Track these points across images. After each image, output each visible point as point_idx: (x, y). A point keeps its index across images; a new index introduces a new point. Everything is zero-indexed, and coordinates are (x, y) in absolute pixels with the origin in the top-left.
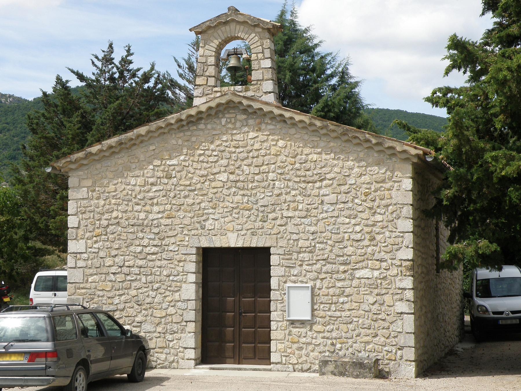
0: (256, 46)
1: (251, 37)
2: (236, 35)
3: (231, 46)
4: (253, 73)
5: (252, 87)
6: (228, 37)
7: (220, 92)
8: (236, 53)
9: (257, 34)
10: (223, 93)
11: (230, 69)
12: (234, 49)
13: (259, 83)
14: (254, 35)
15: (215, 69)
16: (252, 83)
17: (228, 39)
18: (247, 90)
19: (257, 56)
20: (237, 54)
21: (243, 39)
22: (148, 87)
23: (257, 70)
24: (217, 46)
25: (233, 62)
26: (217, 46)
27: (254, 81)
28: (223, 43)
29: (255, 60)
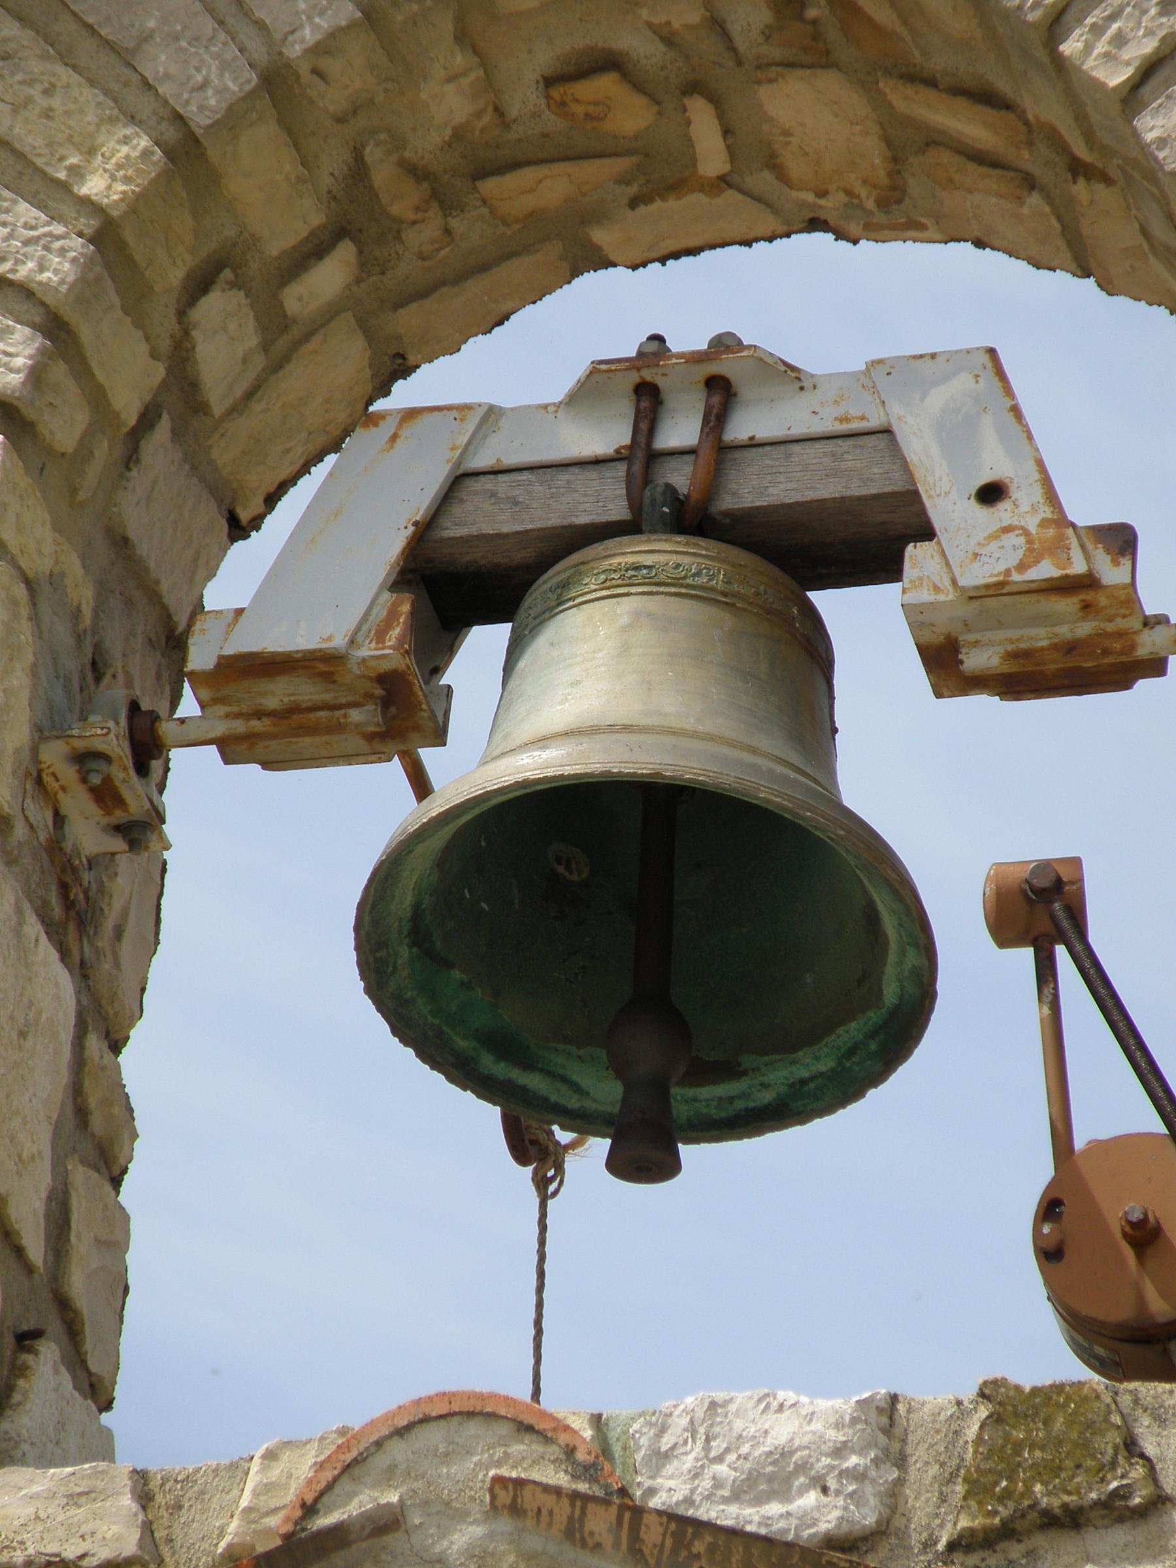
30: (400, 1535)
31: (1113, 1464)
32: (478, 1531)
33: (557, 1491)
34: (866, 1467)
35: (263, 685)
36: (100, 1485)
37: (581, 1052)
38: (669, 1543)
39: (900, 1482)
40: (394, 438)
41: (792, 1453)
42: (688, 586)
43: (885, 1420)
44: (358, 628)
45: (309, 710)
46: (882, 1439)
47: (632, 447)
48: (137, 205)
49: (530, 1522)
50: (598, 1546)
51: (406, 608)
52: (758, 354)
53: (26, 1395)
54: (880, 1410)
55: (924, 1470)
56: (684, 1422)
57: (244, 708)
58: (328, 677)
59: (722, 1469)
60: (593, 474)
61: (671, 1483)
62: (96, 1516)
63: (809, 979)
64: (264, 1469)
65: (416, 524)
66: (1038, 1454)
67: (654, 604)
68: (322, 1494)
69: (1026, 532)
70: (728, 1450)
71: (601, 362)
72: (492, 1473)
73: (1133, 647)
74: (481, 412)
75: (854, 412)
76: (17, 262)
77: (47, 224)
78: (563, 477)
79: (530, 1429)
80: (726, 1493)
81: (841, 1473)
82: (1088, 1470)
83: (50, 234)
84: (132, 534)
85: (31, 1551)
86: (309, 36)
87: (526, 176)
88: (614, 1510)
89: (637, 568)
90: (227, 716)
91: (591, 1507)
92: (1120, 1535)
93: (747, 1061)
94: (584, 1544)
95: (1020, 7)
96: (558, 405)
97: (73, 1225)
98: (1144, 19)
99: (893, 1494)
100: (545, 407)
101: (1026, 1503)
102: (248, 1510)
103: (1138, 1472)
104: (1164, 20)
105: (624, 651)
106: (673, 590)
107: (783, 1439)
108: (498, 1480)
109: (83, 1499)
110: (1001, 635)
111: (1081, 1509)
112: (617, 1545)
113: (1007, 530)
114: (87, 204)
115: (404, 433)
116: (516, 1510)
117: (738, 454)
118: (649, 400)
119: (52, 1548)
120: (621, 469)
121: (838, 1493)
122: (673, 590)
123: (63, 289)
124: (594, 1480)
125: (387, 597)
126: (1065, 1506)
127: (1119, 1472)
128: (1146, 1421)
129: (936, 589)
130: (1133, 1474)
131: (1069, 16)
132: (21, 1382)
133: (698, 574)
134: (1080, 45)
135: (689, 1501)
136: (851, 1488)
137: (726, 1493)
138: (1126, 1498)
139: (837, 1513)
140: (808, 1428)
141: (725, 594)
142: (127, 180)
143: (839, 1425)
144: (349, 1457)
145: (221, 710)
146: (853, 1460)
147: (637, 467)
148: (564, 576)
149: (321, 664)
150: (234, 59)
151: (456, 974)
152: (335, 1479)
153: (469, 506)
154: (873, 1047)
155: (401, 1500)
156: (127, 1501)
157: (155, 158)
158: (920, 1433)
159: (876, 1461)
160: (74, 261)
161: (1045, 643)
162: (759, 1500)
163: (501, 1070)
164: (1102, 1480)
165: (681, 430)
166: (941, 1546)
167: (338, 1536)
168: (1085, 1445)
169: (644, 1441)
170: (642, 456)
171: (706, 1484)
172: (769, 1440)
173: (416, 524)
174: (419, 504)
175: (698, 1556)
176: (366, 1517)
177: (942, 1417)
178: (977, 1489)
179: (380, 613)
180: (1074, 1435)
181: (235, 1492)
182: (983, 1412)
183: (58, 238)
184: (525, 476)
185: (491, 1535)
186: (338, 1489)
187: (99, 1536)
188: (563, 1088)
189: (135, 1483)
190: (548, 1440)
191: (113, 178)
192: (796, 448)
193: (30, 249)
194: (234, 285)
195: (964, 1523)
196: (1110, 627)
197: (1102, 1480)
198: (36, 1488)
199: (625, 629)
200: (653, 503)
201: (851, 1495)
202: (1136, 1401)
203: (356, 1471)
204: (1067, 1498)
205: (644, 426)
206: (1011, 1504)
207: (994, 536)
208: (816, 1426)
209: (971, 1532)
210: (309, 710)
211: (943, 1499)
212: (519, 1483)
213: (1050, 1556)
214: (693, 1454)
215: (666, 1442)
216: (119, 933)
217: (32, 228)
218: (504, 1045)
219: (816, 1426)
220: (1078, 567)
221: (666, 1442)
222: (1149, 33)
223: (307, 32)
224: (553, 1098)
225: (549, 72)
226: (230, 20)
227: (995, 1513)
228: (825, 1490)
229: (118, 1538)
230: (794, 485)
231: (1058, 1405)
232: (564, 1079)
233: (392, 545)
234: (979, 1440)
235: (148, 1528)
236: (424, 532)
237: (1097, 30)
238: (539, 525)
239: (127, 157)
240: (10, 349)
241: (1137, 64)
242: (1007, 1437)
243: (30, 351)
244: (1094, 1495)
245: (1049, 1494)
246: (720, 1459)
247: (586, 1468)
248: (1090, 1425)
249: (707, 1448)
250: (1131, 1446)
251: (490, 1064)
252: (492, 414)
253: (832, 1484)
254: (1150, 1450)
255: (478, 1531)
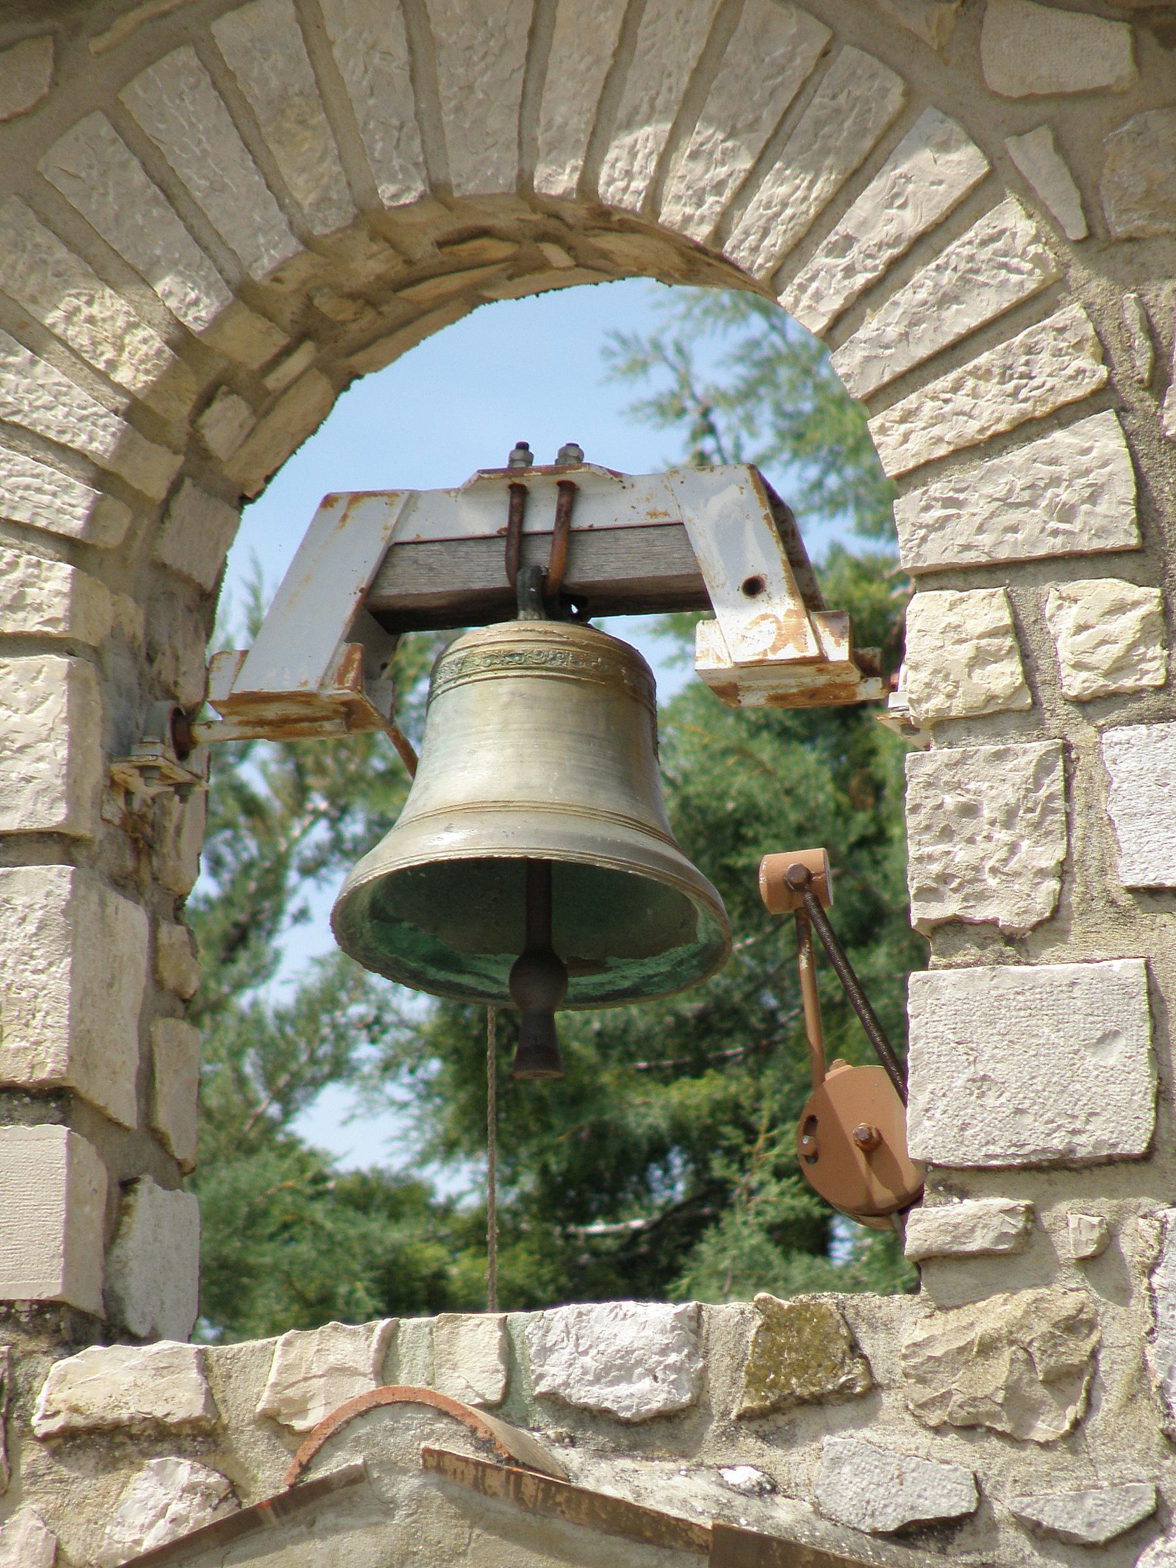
0: (992, 408)
1: (882, 217)
2: (558, 180)
3: (434, 423)
4: (940, 1001)
5: (904, 1329)
6: (372, 221)
7: (202, 1437)
8: (553, 572)
9: (1034, 154)
10: (270, 1477)
11: (422, 920)
12: (515, 483)
13: (1074, 1224)
14: (961, 165)
15: (79, 930)
16: (925, 1227)
17: (369, 264)
18: (802, 1396)
19: (1023, 638)
20: (566, 601)
21: (697, 263)
22: (255, 1004)
23: (1017, 943)
24: (137, 414)
25: (486, 769)
26: (137, 414)
27: (958, 1180)
28: (250, 343)
29: (988, 718)
30: (365, 1484)
31: (843, 1363)
32: (416, 1482)
33: (466, 1460)
34: (682, 1362)
35: (263, 706)
36: (176, 1361)
37: (498, 958)
38: (540, 1495)
39: (705, 1369)
40: (344, 518)
41: (633, 1352)
42: (547, 669)
43: (694, 1324)
44: (326, 674)
45: (296, 721)
46: (693, 1337)
47: (508, 530)
48: (153, 389)
49: (449, 1478)
50: (494, 1494)
51: (357, 656)
52: (593, 469)
53: (130, 1228)
54: (690, 1318)
55: (720, 1362)
56: (562, 1326)
57: (251, 718)
58: (308, 703)
59: (587, 1360)
60: (483, 547)
61: (553, 1370)
62: (175, 1385)
63: (649, 912)
64: (284, 1353)
65: (362, 590)
66: (794, 1355)
67: (522, 685)
68: (312, 1456)
69: (777, 621)
70: (591, 1347)
71: (485, 471)
72: (423, 1445)
73: (854, 695)
74: (404, 497)
75: (660, 509)
76: (74, 434)
77: (94, 405)
78: (463, 549)
79: (446, 1414)
80: (590, 1377)
81: (666, 1367)
82: (826, 1368)
83: (95, 414)
84: (167, 562)
85: (132, 1410)
86: (267, 263)
87: (432, 282)
88: (503, 1474)
89: (512, 656)
90: (240, 723)
91: (488, 1471)
92: (849, 1410)
93: (612, 961)
94: (485, 1493)
95: (750, 269)
96: (457, 490)
97: (157, 1075)
98: (834, 281)
99: (702, 1377)
100: (448, 492)
101: (787, 1392)
102: (275, 1385)
103: (859, 1369)
104: (846, 282)
105: (505, 726)
106: (537, 673)
107: (626, 1342)
108: (427, 1451)
109: (165, 1372)
110: (764, 683)
111: (823, 1395)
112: (507, 1494)
113: (764, 617)
114: (118, 388)
115: (351, 513)
116: (440, 1469)
117: (582, 537)
118: (520, 496)
119: (146, 1409)
120: (502, 545)
121: (664, 1381)
122: (537, 673)
123: (107, 456)
124: (489, 1451)
125: (345, 647)
126: (812, 1394)
127: (846, 1369)
128: (864, 1327)
129: (719, 658)
130: (856, 1371)
131: (784, 274)
132: (126, 1219)
133: (554, 659)
134: (791, 299)
135: (566, 1384)
136: (673, 1377)
137: (590, 1377)
138: (852, 1387)
139: (664, 1396)
140: (643, 1334)
141: (572, 672)
142: (147, 372)
143: (663, 1332)
144: (329, 1431)
145: (235, 719)
146: (673, 1358)
147: (514, 542)
148: (463, 654)
149: (305, 698)
150: (217, 281)
151: (406, 925)
152: (321, 1446)
153: (399, 570)
154: (695, 962)
155: (365, 1463)
156: (194, 1375)
157: (165, 356)
158: (717, 1333)
159: (689, 1356)
160: (113, 434)
161: (794, 690)
162: (614, 1382)
163: (442, 976)
164: (836, 1376)
165: (542, 519)
166: (733, 1416)
167: (324, 1486)
168: (824, 1350)
169: (535, 1340)
170: (516, 538)
171: (577, 1371)
172: (618, 1342)
173: (362, 590)
174: (363, 576)
175: (559, 1504)
176: (342, 1473)
177: (731, 1323)
178: (755, 1380)
179: (340, 660)
180: (817, 1343)
181: (266, 1368)
182: (758, 1321)
183: (102, 416)
184: (436, 547)
185: (424, 1486)
186: (323, 1453)
187: (176, 1400)
188: (487, 982)
189: (199, 1360)
190: (459, 1423)
191: (137, 370)
192: (621, 533)
193: (82, 425)
194: (231, 392)
195: (747, 1404)
196: (838, 680)
197: (836, 1376)
198: (134, 1362)
199: (507, 706)
200: (524, 586)
201: (672, 1382)
202: (857, 1314)
203: (334, 1440)
204: (813, 1389)
205: (516, 519)
206: (777, 1391)
207: (755, 623)
208: (648, 1332)
209: (752, 1410)
210: (296, 721)
211: (734, 1382)
212: (441, 1454)
213: (804, 1425)
214: (567, 1350)
215: (550, 1340)
216: (178, 831)
217: (84, 408)
218: (442, 960)
219: (648, 1332)
220: (812, 651)
221: (550, 1340)
222: (837, 292)
223: (266, 260)
224: (480, 988)
225: (441, 239)
226: (213, 247)
227: (767, 1397)
228: (655, 1378)
229: (190, 1402)
230: (620, 564)
231: (806, 1320)
232: (487, 977)
233: (346, 606)
234: (755, 1343)
235: (209, 1394)
236: (369, 591)
237: (802, 288)
238: (448, 588)
239: (146, 355)
240: (73, 502)
241: (829, 316)
242: (773, 1340)
243: (86, 503)
244: (830, 1387)
245: (801, 1386)
246: (585, 1353)
247: (485, 1442)
248: (827, 1335)
249: (577, 1346)
250: (854, 1346)
251: (433, 973)
252: (413, 497)
253: (660, 1375)
254: (867, 1349)
255: (416, 1482)
